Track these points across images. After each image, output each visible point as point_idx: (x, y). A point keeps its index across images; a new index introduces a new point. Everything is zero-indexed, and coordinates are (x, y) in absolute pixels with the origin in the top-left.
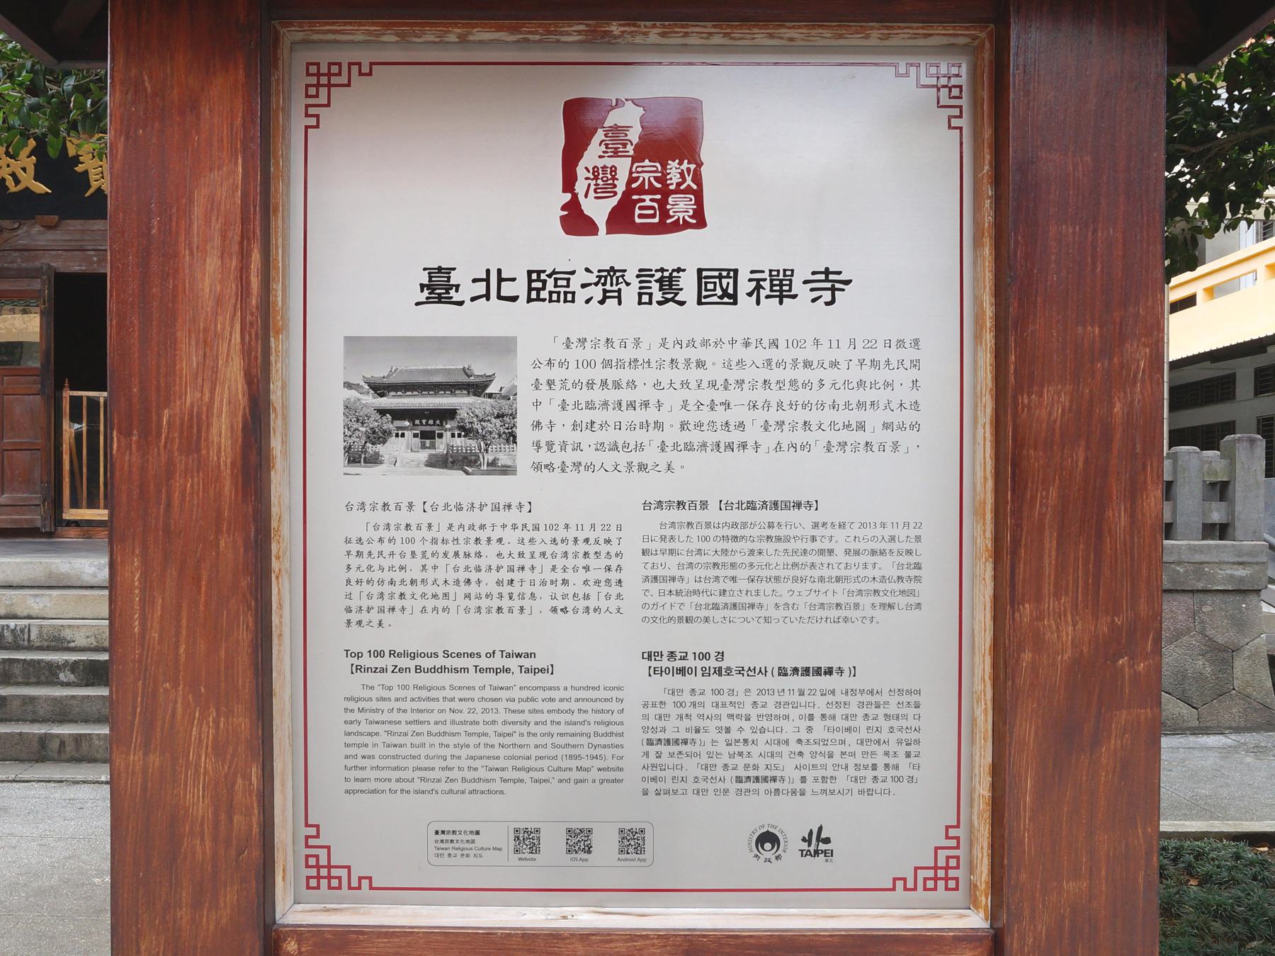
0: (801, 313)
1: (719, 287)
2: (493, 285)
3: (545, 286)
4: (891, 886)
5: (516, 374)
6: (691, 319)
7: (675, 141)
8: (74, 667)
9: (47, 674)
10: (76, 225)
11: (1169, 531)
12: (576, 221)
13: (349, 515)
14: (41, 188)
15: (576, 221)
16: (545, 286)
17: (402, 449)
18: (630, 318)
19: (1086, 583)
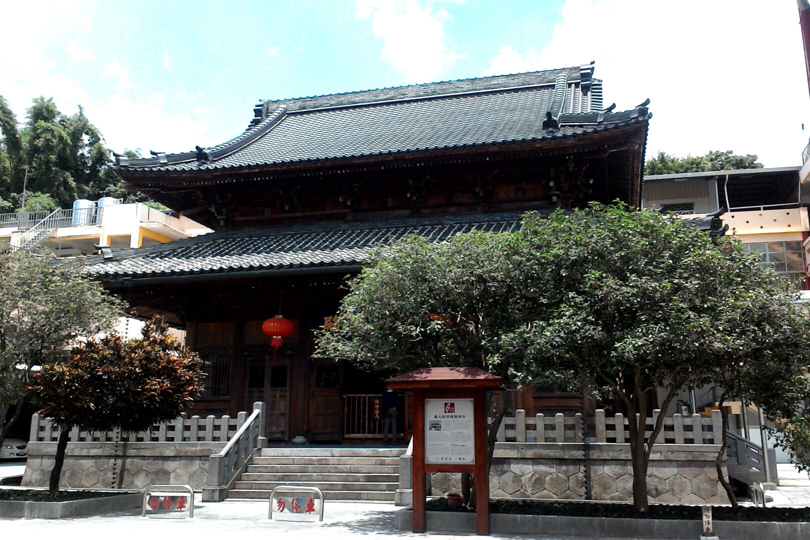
1: (456, 417)
5: (442, 424)
6: (454, 419)
7: (452, 405)
13: (430, 434)
18: (449, 419)
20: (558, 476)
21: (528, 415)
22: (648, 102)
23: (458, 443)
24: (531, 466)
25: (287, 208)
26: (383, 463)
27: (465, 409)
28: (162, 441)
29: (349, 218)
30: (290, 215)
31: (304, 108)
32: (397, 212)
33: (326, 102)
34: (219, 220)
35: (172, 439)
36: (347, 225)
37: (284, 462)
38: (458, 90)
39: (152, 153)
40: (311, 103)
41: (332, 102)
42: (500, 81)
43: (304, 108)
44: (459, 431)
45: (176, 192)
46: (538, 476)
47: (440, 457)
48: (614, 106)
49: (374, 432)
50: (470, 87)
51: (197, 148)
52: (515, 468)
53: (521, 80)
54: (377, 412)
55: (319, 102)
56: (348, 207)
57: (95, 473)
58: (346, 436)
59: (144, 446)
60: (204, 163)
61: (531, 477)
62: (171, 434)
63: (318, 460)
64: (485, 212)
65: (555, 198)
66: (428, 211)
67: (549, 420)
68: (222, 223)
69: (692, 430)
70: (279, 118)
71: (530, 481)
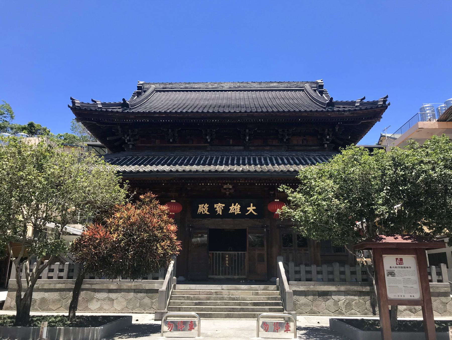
0: (409, 269)
1: (405, 268)
2: (393, 267)
3: (396, 267)
4: (379, 333)
5: (395, 272)
6: (403, 269)
7: (401, 260)
8: (251, 303)
9: (247, 304)
10: (214, 219)
11: (431, 281)
12: (397, 264)
13: (388, 279)
14: (208, 213)
15: (397, 264)
16: (396, 267)
17: (390, 275)
18: (400, 269)
19: (244, 262)
20: (359, 301)
21: (296, 265)
22: (387, 97)
23: (408, 286)
24: (344, 297)
25: (171, 140)
26: (257, 294)
27: (410, 261)
28: (55, 279)
29: (209, 149)
30: (173, 145)
31: (165, 88)
32: (236, 148)
33: (178, 86)
34: (129, 144)
35: (51, 278)
36: (207, 153)
37: (193, 294)
38: (252, 87)
39: (93, 101)
40: (170, 86)
41: (182, 87)
42: (275, 84)
43: (165, 88)
44: (408, 277)
45: (105, 126)
46: (348, 301)
47: (397, 295)
48: (364, 98)
49: (225, 274)
50: (259, 86)
51: (124, 100)
52: (335, 298)
53: (286, 85)
54: (227, 262)
55: (174, 86)
56: (208, 143)
57: (60, 300)
58: (210, 276)
59: (95, 282)
60: (126, 109)
61: (344, 302)
62: (51, 274)
63: (216, 292)
64: (287, 151)
65: (326, 145)
66: (253, 148)
67: (319, 269)
68: (131, 146)
69: (328, 271)
70: (152, 92)
71: (343, 304)
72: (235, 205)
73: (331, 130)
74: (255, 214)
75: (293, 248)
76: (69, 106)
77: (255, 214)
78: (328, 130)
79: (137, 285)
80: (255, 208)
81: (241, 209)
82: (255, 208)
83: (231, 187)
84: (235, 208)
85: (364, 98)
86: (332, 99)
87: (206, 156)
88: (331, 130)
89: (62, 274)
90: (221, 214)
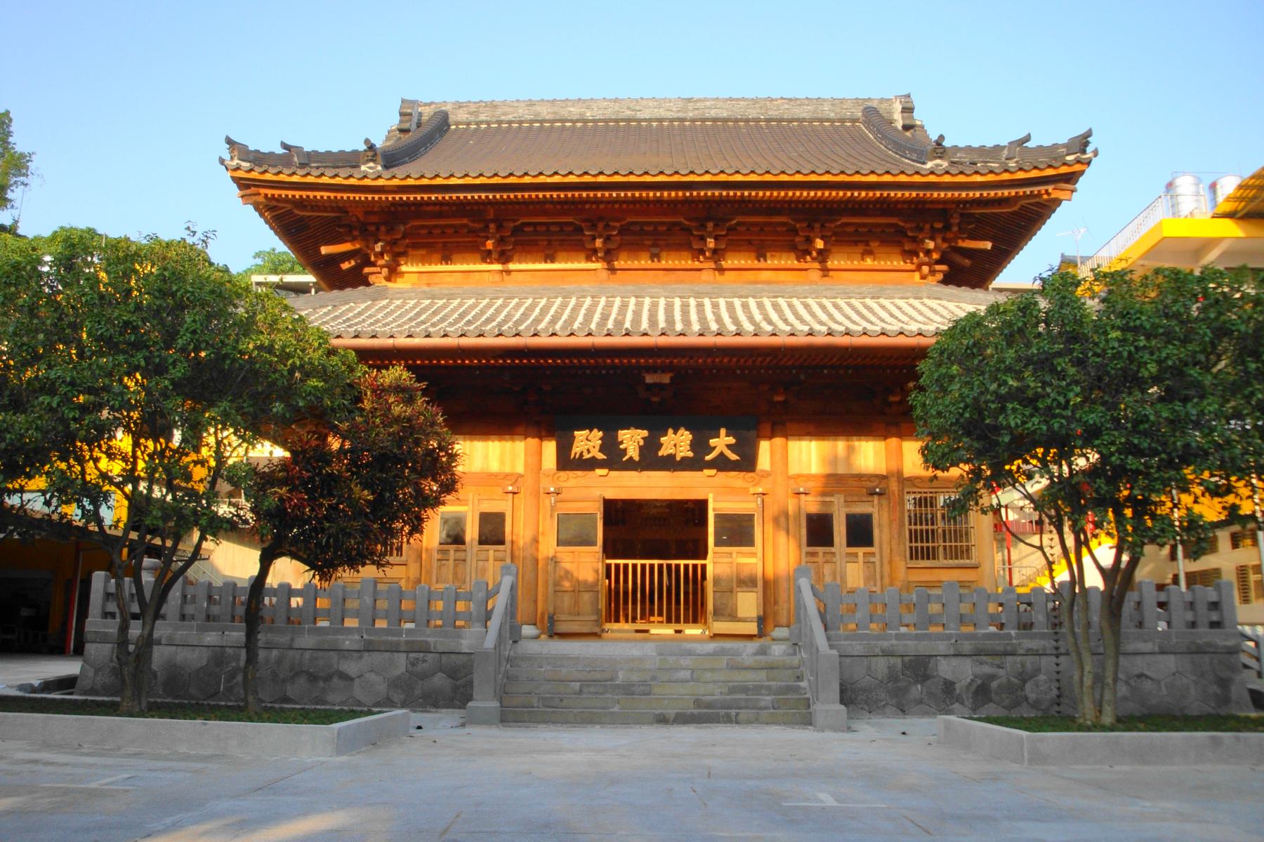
14: (601, 456)
20: (1009, 681)
22: (1089, 134)
39: (285, 146)
48: (1028, 138)
51: (367, 141)
61: (970, 684)
72: (675, 433)
73: (939, 225)
74: (734, 457)
75: (833, 550)
76: (222, 161)
77: (734, 457)
78: (932, 227)
79: (413, 642)
80: (731, 440)
81: (693, 446)
82: (731, 440)
83: (666, 379)
84: (677, 442)
85: (1028, 138)
86: (942, 137)
87: (593, 297)
88: (939, 225)
89: (215, 610)
90: (637, 458)
